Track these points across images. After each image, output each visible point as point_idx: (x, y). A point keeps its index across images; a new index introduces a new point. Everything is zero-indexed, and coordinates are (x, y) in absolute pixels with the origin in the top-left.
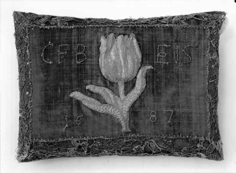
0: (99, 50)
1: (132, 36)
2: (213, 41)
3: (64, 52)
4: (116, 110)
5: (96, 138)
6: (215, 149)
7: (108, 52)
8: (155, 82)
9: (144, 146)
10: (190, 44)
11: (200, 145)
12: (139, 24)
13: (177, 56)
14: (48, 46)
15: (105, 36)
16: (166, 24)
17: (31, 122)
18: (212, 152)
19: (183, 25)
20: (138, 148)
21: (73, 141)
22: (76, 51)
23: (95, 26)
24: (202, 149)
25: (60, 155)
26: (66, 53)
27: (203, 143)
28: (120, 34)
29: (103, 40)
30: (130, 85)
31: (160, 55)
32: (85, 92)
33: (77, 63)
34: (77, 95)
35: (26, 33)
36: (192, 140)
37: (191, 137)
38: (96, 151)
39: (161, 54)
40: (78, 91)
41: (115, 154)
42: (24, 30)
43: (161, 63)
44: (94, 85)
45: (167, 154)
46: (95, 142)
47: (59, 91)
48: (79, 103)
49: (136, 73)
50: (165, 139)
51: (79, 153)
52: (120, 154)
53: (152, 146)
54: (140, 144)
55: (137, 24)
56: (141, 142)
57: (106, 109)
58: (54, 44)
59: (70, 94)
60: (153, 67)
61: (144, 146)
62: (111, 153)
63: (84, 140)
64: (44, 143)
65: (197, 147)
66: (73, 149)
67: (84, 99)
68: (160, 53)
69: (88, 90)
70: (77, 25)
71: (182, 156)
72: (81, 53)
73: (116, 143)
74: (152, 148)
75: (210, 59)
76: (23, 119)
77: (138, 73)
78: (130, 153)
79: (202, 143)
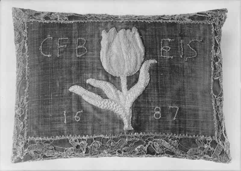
0: (100, 43)
1: (134, 30)
2: (217, 37)
3: (64, 45)
4: (118, 105)
5: (96, 137)
6: (223, 150)
7: (109, 46)
8: (159, 77)
9: (147, 146)
10: (195, 39)
11: (208, 145)
12: (141, 19)
13: (182, 50)
14: (47, 39)
15: (107, 30)
16: (169, 20)
17: (27, 118)
18: (220, 153)
19: (186, 21)
20: (140, 149)
21: (70, 140)
22: (77, 44)
23: (95, 21)
24: (209, 150)
25: (56, 155)
26: (66, 46)
27: (211, 143)
28: (121, 29)
29: (104, 34)
30: (132, 80)
31: (164, 49)
32: (85, 86)
33: (77, 56)
34: (77, 90)
35: (25, 27)
36: (199, 140)
37: (197, 136)
38: (95, 152)
39: (165, 48)
40: (78, 84)
41: (116, 156)
42: (23, 24)
43: (165, 57)
44: (96, 79)
45: (172, 156)
46: (94, 141)
47: (58, 85)
48: (79, 99)
49: (138, 67)
50: (169, 139)
51: (77, 154)
52: (120, 155)
53: (155, 146)
54: (143, 143)
55: (138, 19)
56: (144, 142)
57: (107, 105)
58: (53, 37)
59: (69, 88)
60: (157, 61)
61: (147, 146)
62: (112, 155)
63: (82, 139)
64: (40, 141)
65: (204, 148)
66: (70, 148)
67: (85, 94)
68: (163, 47)
69: (89, 84)
70: (77, 20)
71: (187, 158)
72: (81, 47)
73: (117, 143)
74: (155, 147)
75: (215, 55)
76: (19, 115)
77: (141, 67)
78: (131, 154)
79: (210, 143)
